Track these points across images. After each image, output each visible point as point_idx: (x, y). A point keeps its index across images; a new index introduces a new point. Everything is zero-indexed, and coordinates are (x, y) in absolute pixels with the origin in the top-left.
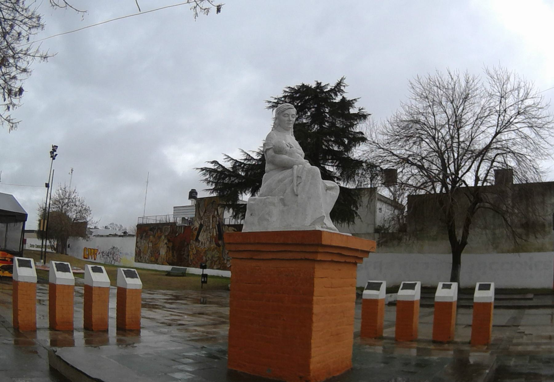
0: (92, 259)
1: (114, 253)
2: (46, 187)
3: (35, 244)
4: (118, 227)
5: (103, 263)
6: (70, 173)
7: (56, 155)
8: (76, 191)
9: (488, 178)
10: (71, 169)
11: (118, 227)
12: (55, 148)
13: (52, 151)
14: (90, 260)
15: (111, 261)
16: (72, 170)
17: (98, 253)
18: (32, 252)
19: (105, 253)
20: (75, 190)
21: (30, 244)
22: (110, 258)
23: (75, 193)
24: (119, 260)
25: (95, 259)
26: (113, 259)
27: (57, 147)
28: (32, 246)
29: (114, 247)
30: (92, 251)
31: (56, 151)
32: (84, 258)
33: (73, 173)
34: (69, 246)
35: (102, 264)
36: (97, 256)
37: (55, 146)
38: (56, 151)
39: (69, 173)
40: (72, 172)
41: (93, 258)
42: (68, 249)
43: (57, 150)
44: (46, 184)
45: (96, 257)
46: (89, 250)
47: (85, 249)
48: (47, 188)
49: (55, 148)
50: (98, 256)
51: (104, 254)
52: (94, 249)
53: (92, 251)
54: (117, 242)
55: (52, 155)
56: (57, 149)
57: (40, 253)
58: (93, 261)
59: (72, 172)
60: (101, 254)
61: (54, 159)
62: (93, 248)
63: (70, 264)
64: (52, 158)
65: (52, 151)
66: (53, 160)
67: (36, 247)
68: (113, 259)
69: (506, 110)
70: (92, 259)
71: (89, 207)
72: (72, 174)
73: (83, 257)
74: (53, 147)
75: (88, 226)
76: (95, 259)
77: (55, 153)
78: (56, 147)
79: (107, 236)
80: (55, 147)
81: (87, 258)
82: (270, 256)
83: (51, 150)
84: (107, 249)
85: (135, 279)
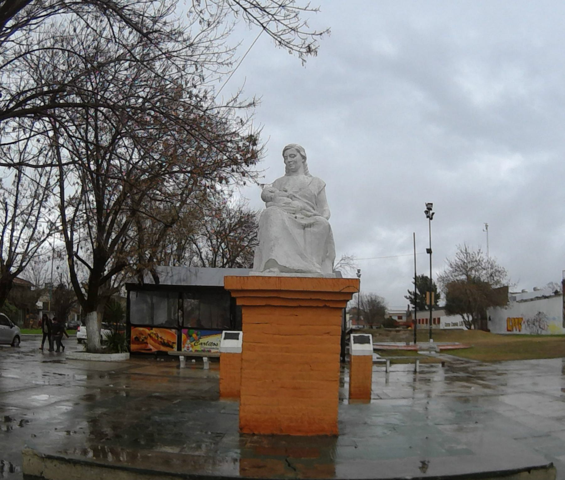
0: (516, 330)
1: (540, 320)
2: (428, 253)
3: (450, 323)
4: (559, 286)
5: (529, 334)
6: (485, 230)
7: (433, 214)
8: (481, 251)
9: (78, 214)
10: (485, 225)
11: (559, 286)
12: (429, 207)
13: (427, 210)
14: (515, 332)
15: (538, 330)
16: (487, 226)
17: (523, 322)
18: (424, 331)
19: (530, 321)
20: (480, 250)
21: (446, 323)
22: (536, 326)
23: (480, 254)
24: (546, 328)
25: (520, 331)
26: (540, 327)
27: (432, 204)
28: (447, 325)
29: (540, 313)
30: (516, 320)
31: (431, 209)
32: (508, 330)
33: (488, 229)
34: (490, 319)
35: (528, 335)
36: (522, 327)
37: (429, 204)
38: (431, 209)
39: (484, 231)
40: (487, 229)
41: (518, 330)
42: (489, 323)
43: (433, 209)
44: (427, 250)
45: (521, 328)
46: (513, 320)
47: (509, 319)
48: (429, 254)
49: (429, 207)
50: (523, 326)
51: (529, 323)
52: (518, 319)
53: (516, 320)
54: (542, 305)
55: (428, 215)
56: (432, 207)
57: (429, 331)
58: (518, 332)
59: (487, 229)
60: (526, 323)
61: (431, 219)
62: (517, 317)
63: (373, 336)
64: (428, 219)
65: (427, 210)
66: (431, 221)
67: (452, 326)
68: (540, 327)
69: (126, 150)
70: (516, 330)
71: (503, 268)
72: (487, 231)
73: (506, 330)
74: (427, 205)
75: (510, 291)
76: (520, 331)
77: (431, 212)
78: (431, 205)
79: (532, 300)
80: (429, 205)
81: (510, 331)
82: (313, 297)
83: (426, 209)
84: (532, 315)
85: (367, 345)
